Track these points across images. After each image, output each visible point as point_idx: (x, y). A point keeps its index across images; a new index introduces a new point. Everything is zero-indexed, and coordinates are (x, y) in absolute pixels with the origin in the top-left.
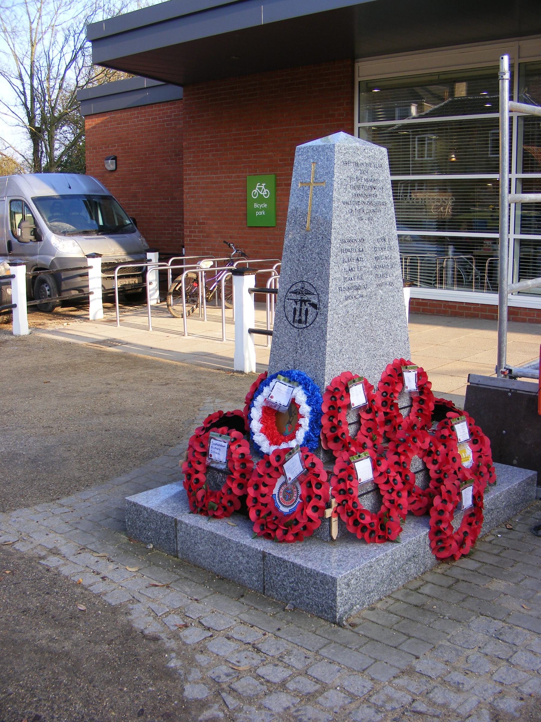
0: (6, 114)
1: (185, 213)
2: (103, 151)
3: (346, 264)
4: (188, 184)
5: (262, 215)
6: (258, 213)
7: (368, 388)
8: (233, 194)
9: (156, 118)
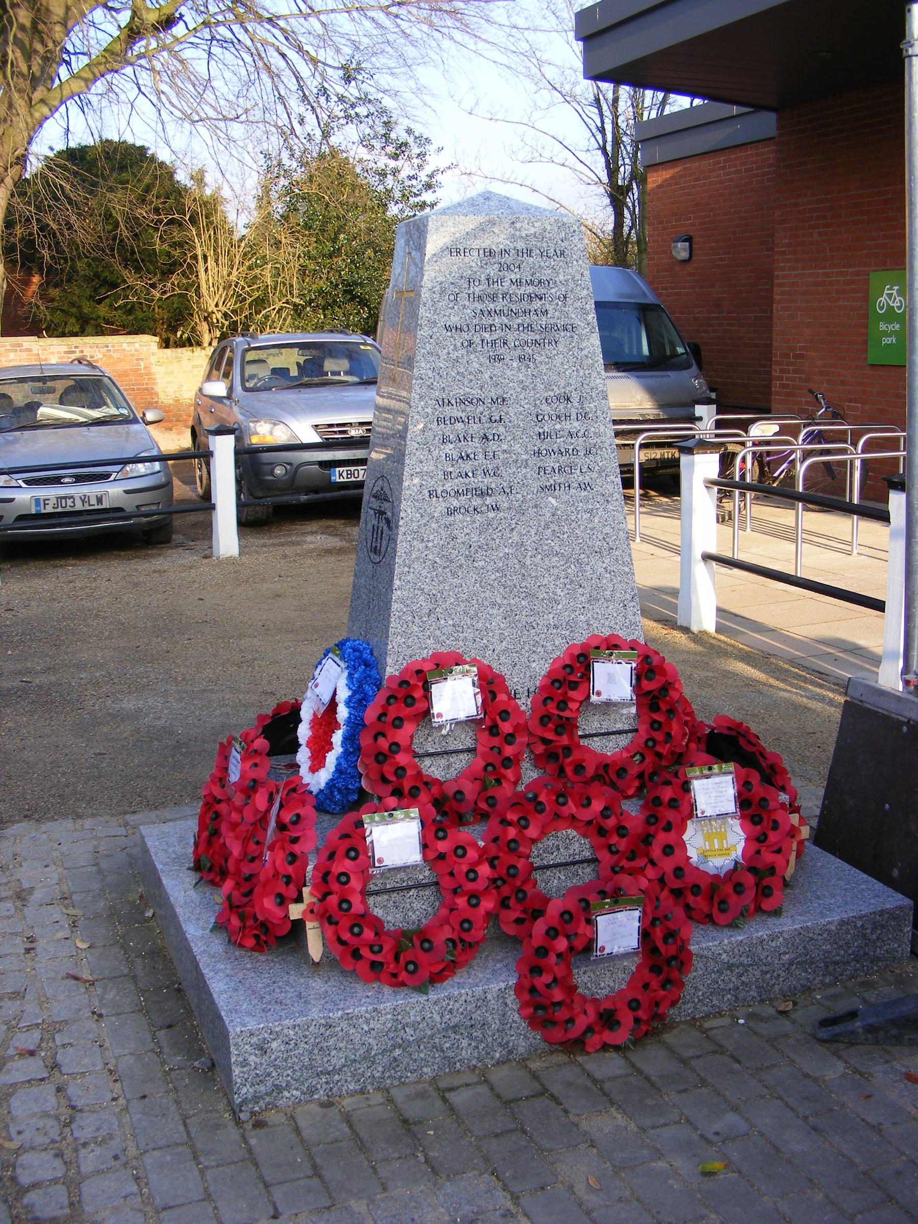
0: (563, 165)
1: (774, 336)
2: (673, 227)
3: (451, 446)
4: (781, 285)
5: (892, 344)
6: (886, 341)
7: (490, 685)
8: (847, 303)
9: (751, 169)
